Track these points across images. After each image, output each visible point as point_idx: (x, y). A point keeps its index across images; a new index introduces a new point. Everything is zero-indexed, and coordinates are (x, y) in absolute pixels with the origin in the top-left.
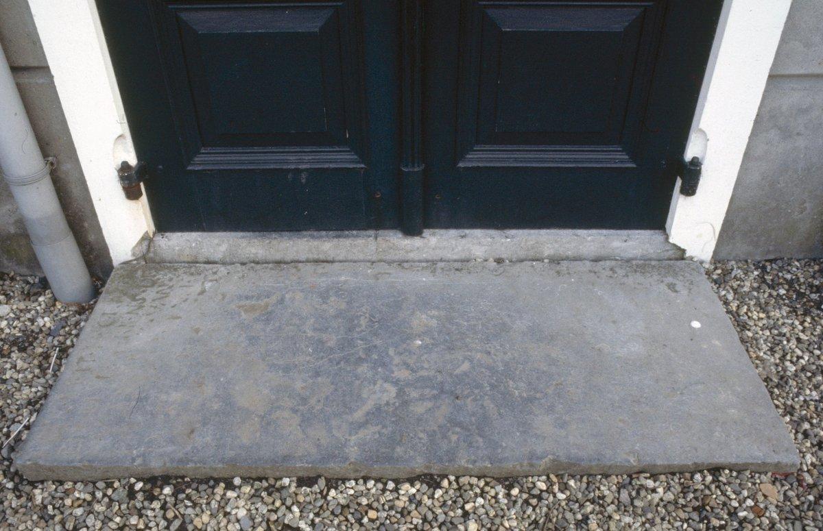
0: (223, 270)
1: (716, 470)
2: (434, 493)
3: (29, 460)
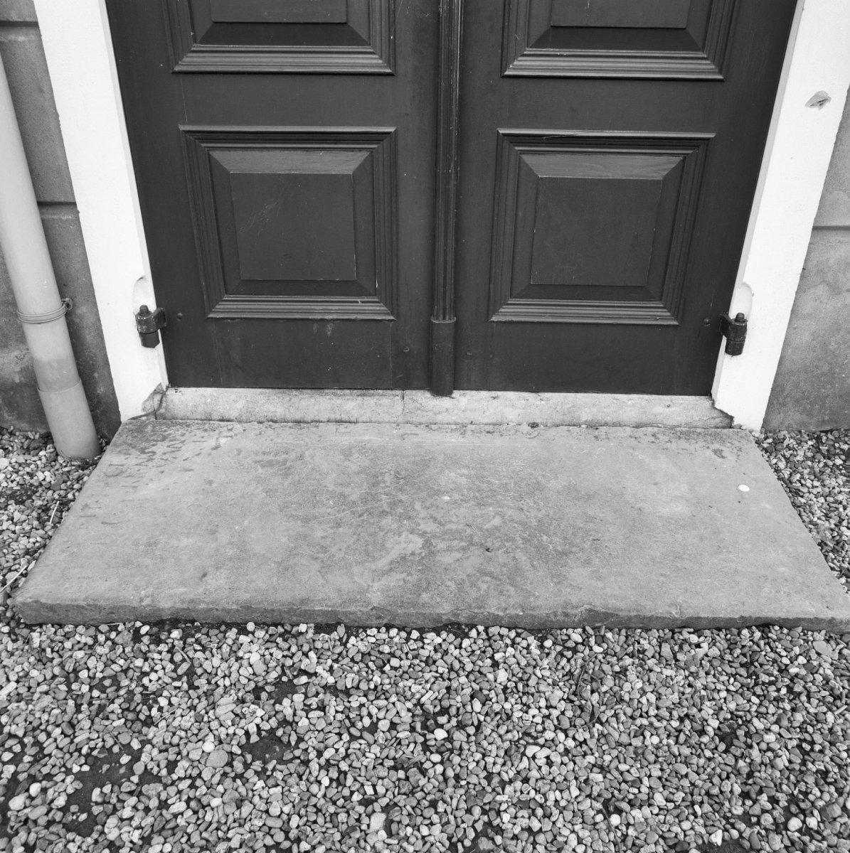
0: (238, 427)
1: (765, 625)
2: (461, 644)
3: (30, 598)
